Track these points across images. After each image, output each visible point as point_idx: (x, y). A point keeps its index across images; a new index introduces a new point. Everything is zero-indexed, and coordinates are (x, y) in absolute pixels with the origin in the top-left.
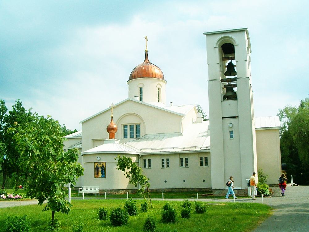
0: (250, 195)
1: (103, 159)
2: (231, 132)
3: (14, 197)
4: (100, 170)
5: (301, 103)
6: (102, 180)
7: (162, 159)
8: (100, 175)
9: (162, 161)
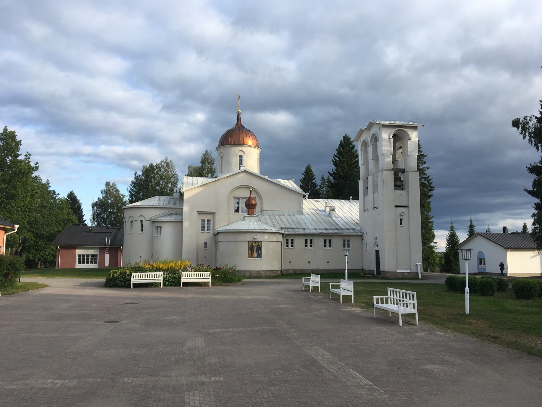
0: (497, 227)
1: (259, 237)
2: (401, 220)
6: (258, 260)
7: (343, 240)
8: (255, 254)
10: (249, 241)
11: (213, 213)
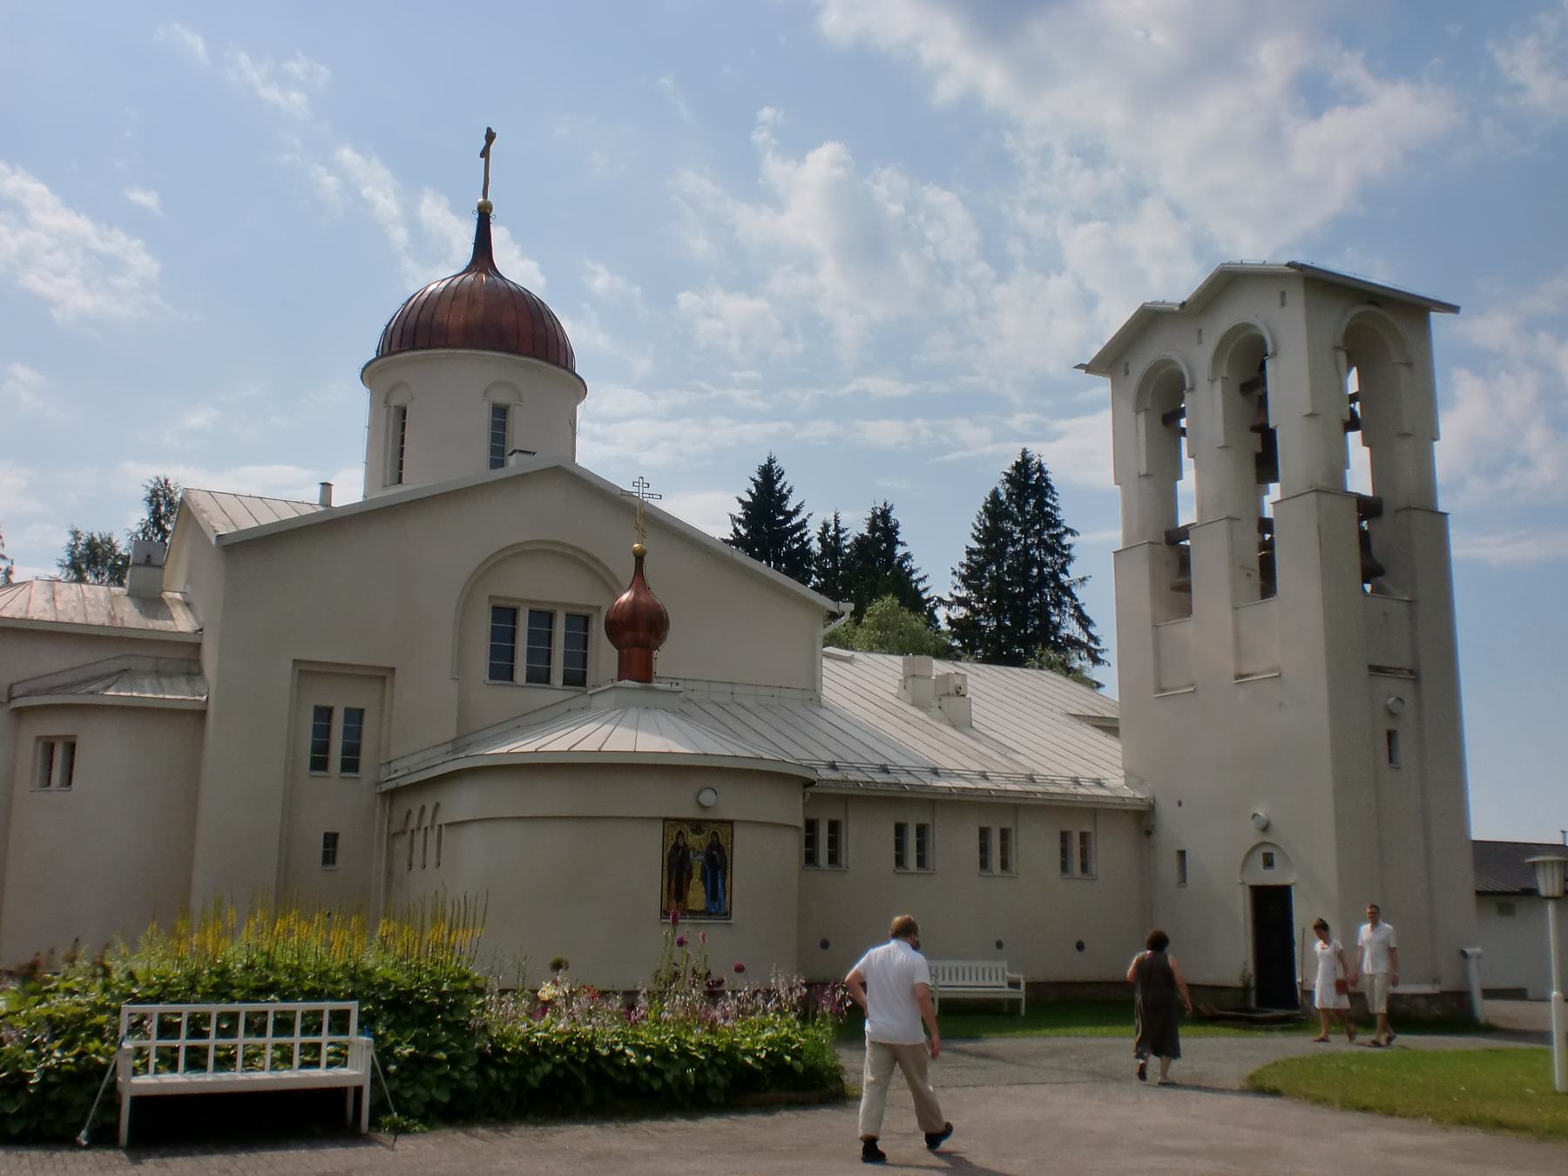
1: (726, 803)
2: (1391, 735)
3: (950, 1091)
4: (697, 872)
5: (69, 538)
8: (697, 895)
9: (326, 845)
10: (665, 820)
11: (382, 676)
